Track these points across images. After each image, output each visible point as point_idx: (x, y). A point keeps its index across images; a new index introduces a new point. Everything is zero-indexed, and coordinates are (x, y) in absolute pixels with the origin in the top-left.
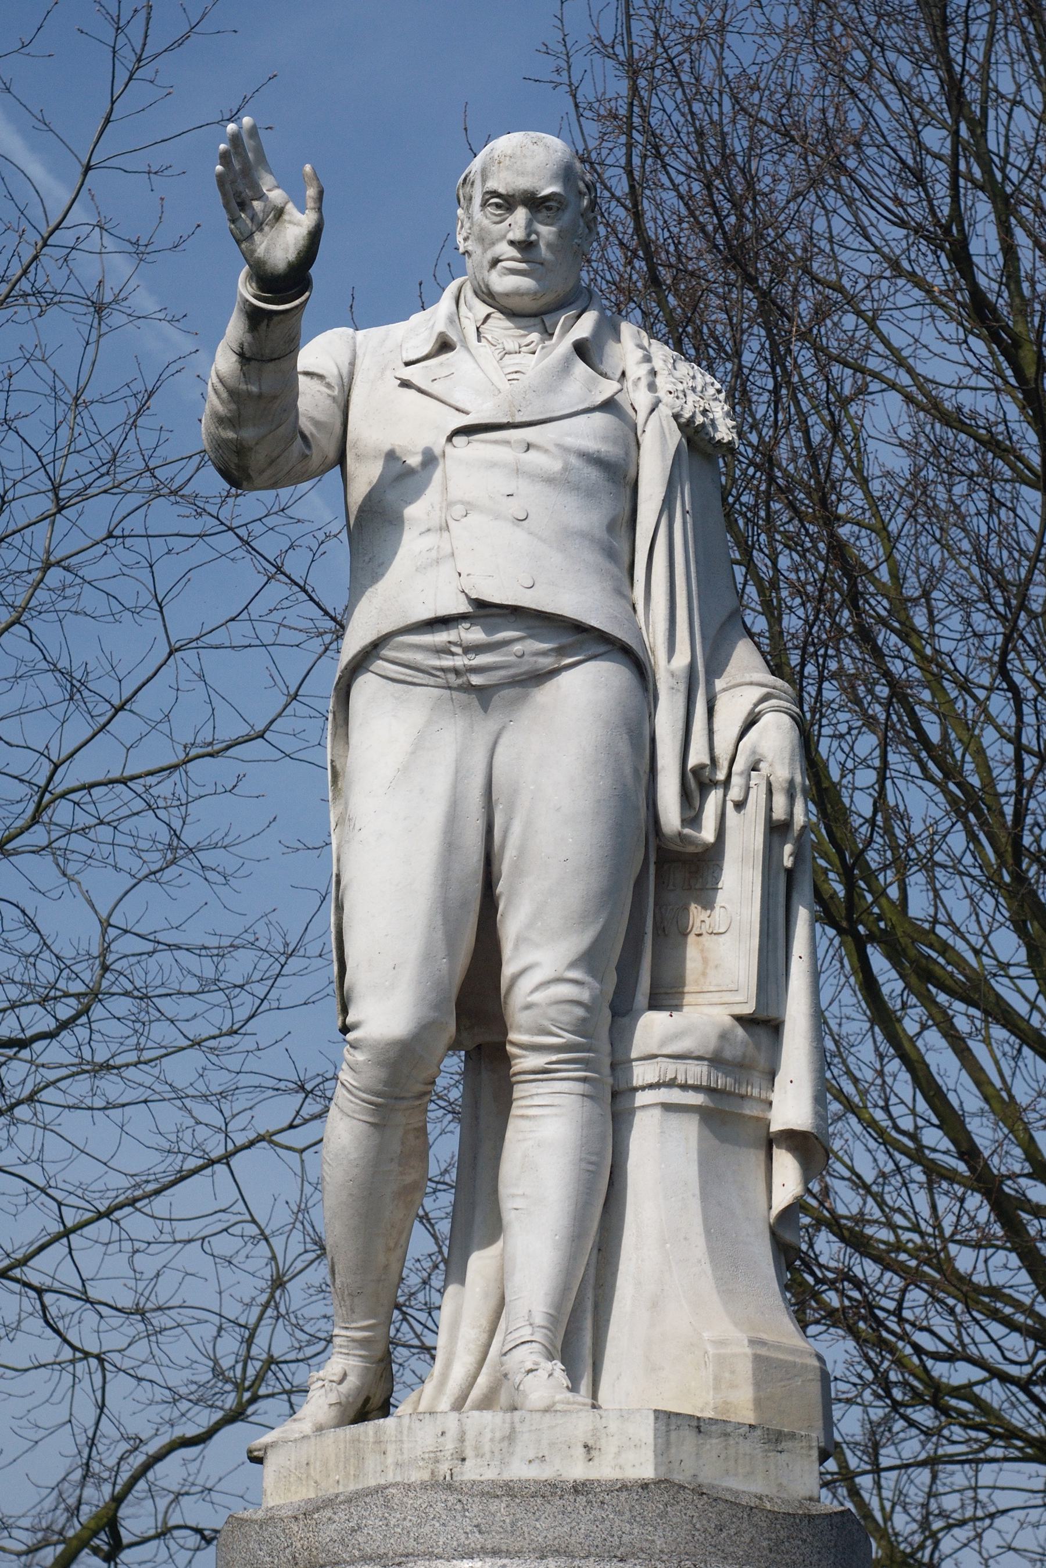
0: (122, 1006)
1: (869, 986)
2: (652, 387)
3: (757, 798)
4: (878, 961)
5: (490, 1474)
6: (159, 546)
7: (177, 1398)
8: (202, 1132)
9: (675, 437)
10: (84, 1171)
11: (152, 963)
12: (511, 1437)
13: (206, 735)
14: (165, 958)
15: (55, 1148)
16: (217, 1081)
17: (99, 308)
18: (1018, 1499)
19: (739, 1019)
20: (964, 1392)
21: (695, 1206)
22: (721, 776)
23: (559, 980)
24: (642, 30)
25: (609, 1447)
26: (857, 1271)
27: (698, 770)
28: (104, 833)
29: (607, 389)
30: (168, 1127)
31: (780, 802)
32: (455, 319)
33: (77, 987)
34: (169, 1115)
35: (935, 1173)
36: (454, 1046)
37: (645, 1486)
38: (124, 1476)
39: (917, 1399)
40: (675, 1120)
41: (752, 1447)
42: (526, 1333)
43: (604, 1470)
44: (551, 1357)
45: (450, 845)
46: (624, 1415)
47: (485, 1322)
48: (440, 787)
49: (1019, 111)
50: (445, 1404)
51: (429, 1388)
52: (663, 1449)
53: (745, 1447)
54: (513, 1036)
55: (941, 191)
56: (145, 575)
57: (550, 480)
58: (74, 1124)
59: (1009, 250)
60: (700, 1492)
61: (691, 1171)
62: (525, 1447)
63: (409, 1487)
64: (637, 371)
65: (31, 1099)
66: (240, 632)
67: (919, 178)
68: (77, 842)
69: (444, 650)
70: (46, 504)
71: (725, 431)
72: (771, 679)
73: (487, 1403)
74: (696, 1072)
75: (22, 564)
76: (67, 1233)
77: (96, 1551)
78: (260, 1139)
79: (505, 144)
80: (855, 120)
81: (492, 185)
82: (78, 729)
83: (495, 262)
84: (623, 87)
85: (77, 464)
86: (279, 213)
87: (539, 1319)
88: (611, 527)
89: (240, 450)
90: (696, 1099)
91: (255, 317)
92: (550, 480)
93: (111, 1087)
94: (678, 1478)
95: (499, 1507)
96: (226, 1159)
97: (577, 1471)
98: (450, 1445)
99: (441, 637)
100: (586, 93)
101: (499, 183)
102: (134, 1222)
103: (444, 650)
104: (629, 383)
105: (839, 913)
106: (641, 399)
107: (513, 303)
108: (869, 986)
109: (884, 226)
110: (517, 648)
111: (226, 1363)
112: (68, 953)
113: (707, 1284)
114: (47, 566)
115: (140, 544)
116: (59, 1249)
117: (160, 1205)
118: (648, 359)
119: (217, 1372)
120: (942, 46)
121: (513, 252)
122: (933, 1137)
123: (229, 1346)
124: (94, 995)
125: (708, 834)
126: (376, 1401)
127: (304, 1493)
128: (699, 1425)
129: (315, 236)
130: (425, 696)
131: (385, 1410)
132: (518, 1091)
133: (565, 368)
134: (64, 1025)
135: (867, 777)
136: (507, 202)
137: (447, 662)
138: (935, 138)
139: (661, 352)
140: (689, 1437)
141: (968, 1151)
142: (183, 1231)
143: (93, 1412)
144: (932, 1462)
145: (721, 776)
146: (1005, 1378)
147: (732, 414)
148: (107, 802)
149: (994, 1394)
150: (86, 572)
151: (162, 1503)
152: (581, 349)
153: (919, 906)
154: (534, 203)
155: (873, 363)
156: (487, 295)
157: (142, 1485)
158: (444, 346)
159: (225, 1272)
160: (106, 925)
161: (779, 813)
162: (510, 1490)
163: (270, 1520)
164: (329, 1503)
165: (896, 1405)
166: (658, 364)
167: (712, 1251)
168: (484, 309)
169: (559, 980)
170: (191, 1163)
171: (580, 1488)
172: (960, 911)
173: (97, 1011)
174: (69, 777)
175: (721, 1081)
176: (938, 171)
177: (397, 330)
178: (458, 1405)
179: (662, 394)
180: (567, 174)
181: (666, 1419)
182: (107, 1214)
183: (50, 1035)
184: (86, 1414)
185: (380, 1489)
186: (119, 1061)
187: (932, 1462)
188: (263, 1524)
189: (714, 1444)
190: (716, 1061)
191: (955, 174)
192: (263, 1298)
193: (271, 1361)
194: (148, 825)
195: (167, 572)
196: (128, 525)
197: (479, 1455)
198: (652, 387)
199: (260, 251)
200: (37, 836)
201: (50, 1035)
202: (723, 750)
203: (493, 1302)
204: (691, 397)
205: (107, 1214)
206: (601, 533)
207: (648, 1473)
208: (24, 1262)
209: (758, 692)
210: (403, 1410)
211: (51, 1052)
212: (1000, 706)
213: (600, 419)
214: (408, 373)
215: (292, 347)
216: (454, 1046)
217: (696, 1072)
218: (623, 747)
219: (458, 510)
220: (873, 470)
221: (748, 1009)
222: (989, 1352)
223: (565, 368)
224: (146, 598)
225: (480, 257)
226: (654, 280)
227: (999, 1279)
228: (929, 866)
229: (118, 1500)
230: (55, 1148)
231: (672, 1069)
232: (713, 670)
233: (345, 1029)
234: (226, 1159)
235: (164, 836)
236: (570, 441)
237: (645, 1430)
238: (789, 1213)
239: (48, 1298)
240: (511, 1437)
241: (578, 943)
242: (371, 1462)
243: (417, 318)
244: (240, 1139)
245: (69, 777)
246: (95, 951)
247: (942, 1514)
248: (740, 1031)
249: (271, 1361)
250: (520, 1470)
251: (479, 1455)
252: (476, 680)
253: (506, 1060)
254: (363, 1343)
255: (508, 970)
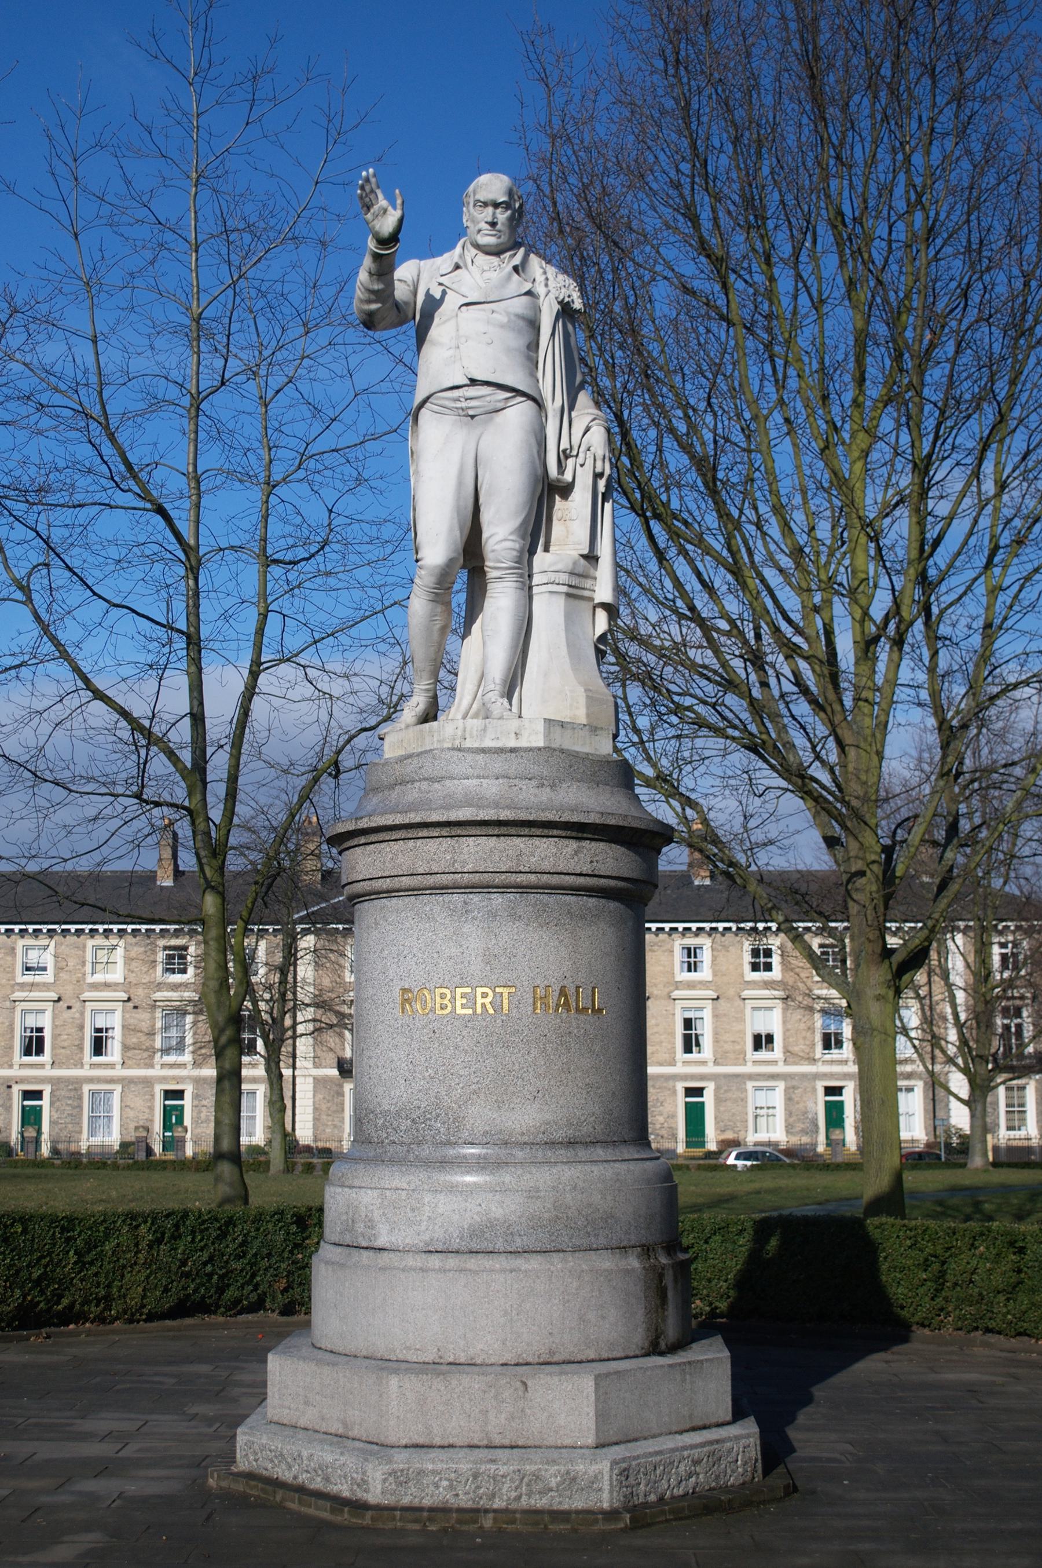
0: (336, 547)
1: (651, 537)
2: (546, 285)
3: (589, 462)
4: (656, 527)
5: (476, 745)
6: (349, 349)
7: (362, 711)
8: (372, 601)
9: (556, 307)
10: (322, 617)
11: (349, 528)
12: (485, 730)
13: (371, 431)
14: (356, 526)
15: (309, 607)
16: (379, 580)
17: (323, 244)
18: (715, 753)
19: (582, 556)
20: (689, 709)
21: (563, 634)
22: (574, 453)
23: (505, 540)
24: (557, 123)
25: (525, 734)
26: (644, 659)
27: (564, 451)
28: (327, 473)
29: (527, 286)
30: (357, 599)
31: (599, 464)
32: (462, 256)
33: (320, 539)
34: (357, 594)
35: (681, 616)
36: (463, 567)
37: (539, 749)
38: (341, 743)
39: (671, 712)
40: (554, 598)
41: (585, 732)
42: (492, 687)
43: (523, 743)
44: (502, 697)
45: (460, 483)
46: (531, 721)
47: (476, 683)
48: (455, 457)
49: (722, 156)
50: (459, 716)
51: (453, 709)
52: (547, 734)
53: (581, 733)
54: (487, 563)
55: (687, 192)
56: (344, 362)
57: (502, 326)
58: (318, 597)
59: (716, 220)
60: (562, 751)
61: (561, 619)
62: (491, 734)
63: (443, 750)
64: (540, 278)
65: (299, 586)
66: (385, 386)
67: (677, 186)
68: (318, 478)
69: (458, 400)
70: (301, 330)
71: (578, 305)
72: (596, 412)
73: (476, 716)
74: (564, 578)
75: (291, 357)
76: (315, 642)
77: (330, 774)
78: (395, 603)
79: (484, 178)
80: (651, 159)
81: (479, 197)
82: (317, 428)
83: (479, 231)
84: (549, 147)
85: (315, 313)
86: (385, 211)
87: (498, 681)
88: (529, 347)
89: (371, 314)
90: (565, 589)
91: (376, 257)
92: (502, 326)
93: (332, 581)
94: (553, 746)
95: (480, 757)
96: (382, 611)
97: (512, 743)
98: (459, 733)
99: (456, 393)
100: (534, 148)
101: (482, 196)
102: (343, 638)
103: (458, 400)
104: (537, 284)
105: (638, 507)
106: (540, 290)
107: (488, 249)
108: (651, 537)
109: (662, 208)
110: (488, 399)
111: (383, 697)
112: (314, 524)
113: (567, 666)
114: (303, 358)
115: (341, 348)
116: (312, 649)
117: (354, 632)
118: (545, 273)
119: (381, 701)
120: (688, 125)
121: (488, 227)
122: (679, 603)
123: (385, 690)
124: (326, 543)
125: (568, 477)
126: (431, 715)
127: (401, 752)
128: (562, 725)
129: (401, 221)
130: (450, 419)
131: (435, 718)
132: (489, 586)
133: (509, 278)
134: (313, 556)
135: (652, 448)
136: (485, 204)
137: (459, 405)
138: (685, 167)
139: (551, 270)
140: (558, 729)
141: (692, 608)
142: (364, 643)
143: (327, 717)
144: (678, 737)
145: (574, 453)
146: (705, 703)
147: (582, 297)
148: (329, 459)
149: (700, 709)
150: (320, 360)
151: (358, 755)
152: (516, 269)
153: (675, 504)
154: (496, 205)
155: (659, 268)
156: (477, 246)
157: (348, 747)
158: (457, 267)
159: (383, 658)
160: (331, 511)
161: (599, 470)
162: (484, 751)
163: (387, 763)
164: (410, 756)
165: (660, 715)
166: (549, 276)
167: (569, 653)
168: (474, 251)
169: (505, 540)
170: (367, 613)
171: (513, 750)
172: (692, 506)
173: (327, 549)
174: (313, 449)
175: (574, 581)
176: (686, 181)
177: (438, 260)
178: (465, 717)
179: (551, 288)
180: (510, 193)
181: (549, 722)
182: (332, 634)
183: (307, 559)
184: (324, 717)
185: (431, 750)
186: (336, 570)
187: (678, 737)
188: (383, 765)
189: (568, 733)
190: (572, 573)
191: (693, 183)
192: (398, 671)
193: (402, 695)
194: (347, 469)
195: (354, 360)
196: (335, 341)
197: (472, 737)
198: (546, 285)
199: (377, 228)
200: (301, 474)
201: (307, 559)
202: (575, 442)
203: (479, 674)
204: (563, 290)
205: (332, 634)
206: (524, 349)
207: (541, 744)
208: (296, 655)
209: (591, 418)
210: (441, 717)
211: (308, 567)
212: (709, 418)
213: (525, 299)
214: (442, 280)
215: (391, 269)
216: (463, 567)
217: (564, 578)
218: (533, 441)
219: (463, 340)
220: (658, 314)
221: (586, 552)
222: (699, 692)
223: (509, 278)
224: (345, 372)
225: (472, 229)
226: (561, 231)
227: (707, 662)
228: (679, 486)
229: (339, 752)
230: (309, 607)
231: (553, 577)
232: (571, 408)
233: (417, 561)
234: (382, 611)
235: (355, 474)
236: (511, 310)
237: (540, 727)
238: (602, 638)
239: (308, 670)
240: (485, 730)
241: (516, 522)
242: (427, 740)
243: (446, 255)
244: (387, 603)
245: (313, 449)
246: (326, 523)
247: (684, 759)
248: (582, 561)
249: (402, 695)
250: (488, 743)
251: (472, 737)
252: (471, 412)
253: (484, 573)
254: (427, 690)
255: (485, 536)
